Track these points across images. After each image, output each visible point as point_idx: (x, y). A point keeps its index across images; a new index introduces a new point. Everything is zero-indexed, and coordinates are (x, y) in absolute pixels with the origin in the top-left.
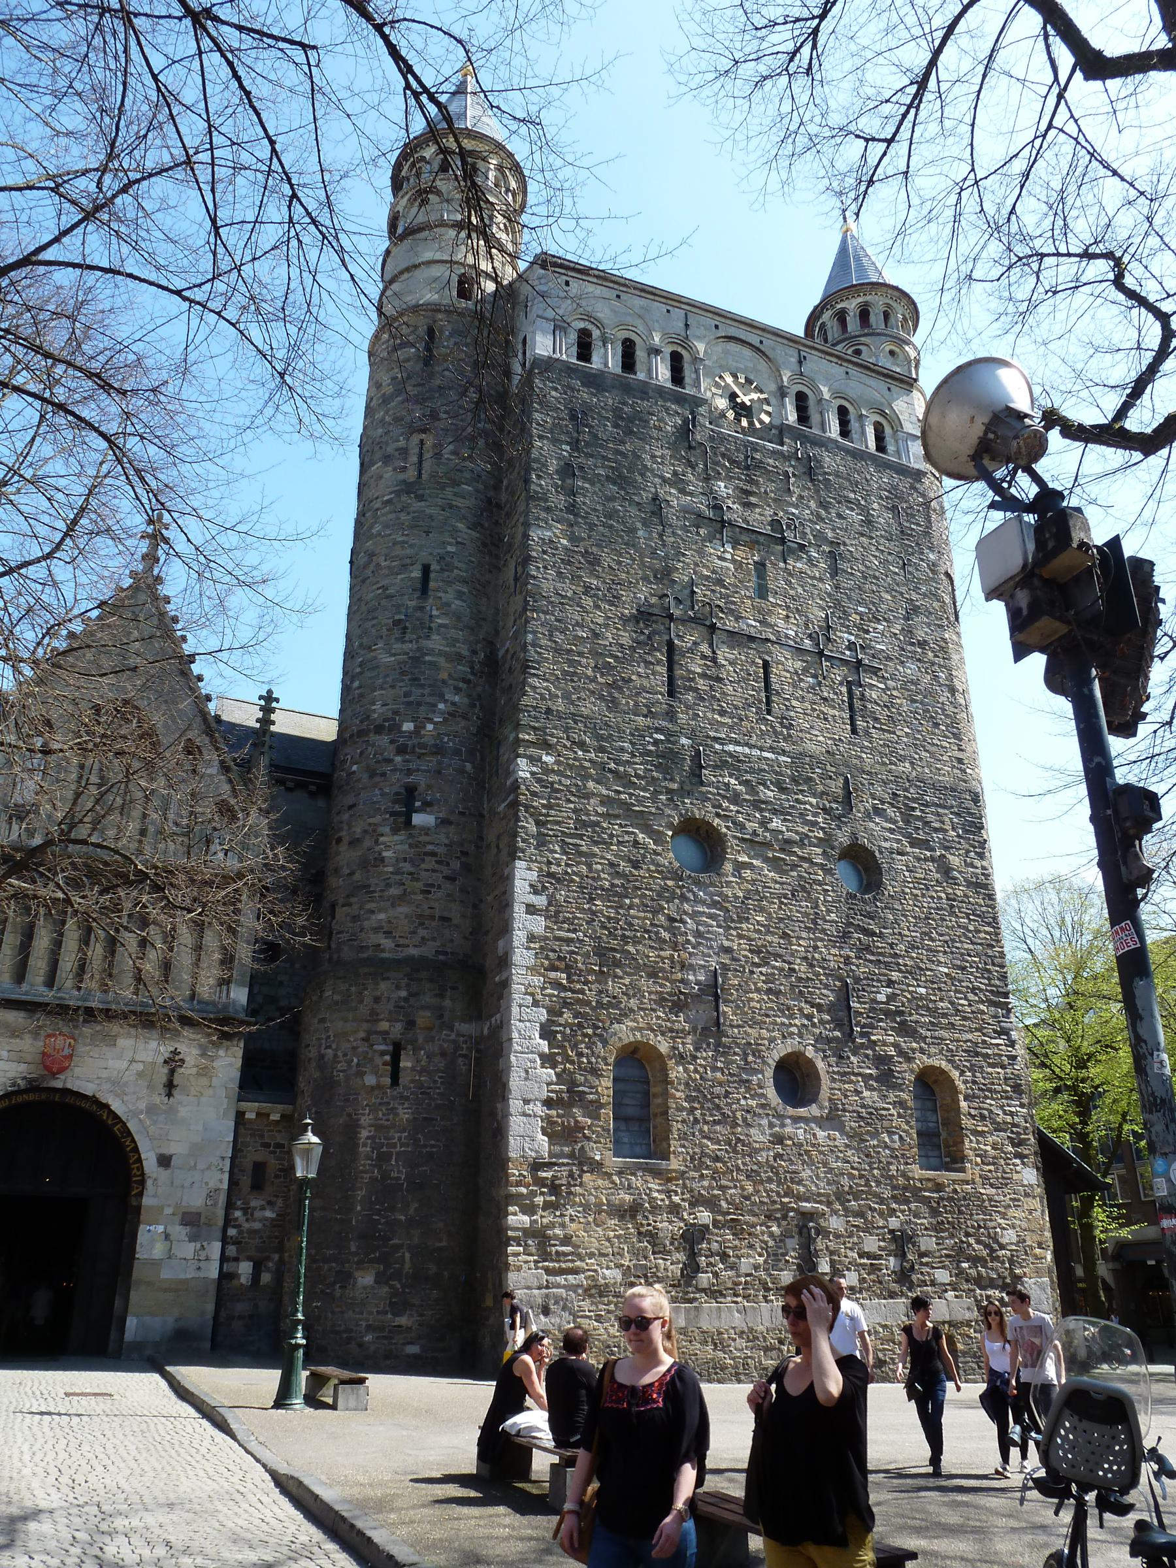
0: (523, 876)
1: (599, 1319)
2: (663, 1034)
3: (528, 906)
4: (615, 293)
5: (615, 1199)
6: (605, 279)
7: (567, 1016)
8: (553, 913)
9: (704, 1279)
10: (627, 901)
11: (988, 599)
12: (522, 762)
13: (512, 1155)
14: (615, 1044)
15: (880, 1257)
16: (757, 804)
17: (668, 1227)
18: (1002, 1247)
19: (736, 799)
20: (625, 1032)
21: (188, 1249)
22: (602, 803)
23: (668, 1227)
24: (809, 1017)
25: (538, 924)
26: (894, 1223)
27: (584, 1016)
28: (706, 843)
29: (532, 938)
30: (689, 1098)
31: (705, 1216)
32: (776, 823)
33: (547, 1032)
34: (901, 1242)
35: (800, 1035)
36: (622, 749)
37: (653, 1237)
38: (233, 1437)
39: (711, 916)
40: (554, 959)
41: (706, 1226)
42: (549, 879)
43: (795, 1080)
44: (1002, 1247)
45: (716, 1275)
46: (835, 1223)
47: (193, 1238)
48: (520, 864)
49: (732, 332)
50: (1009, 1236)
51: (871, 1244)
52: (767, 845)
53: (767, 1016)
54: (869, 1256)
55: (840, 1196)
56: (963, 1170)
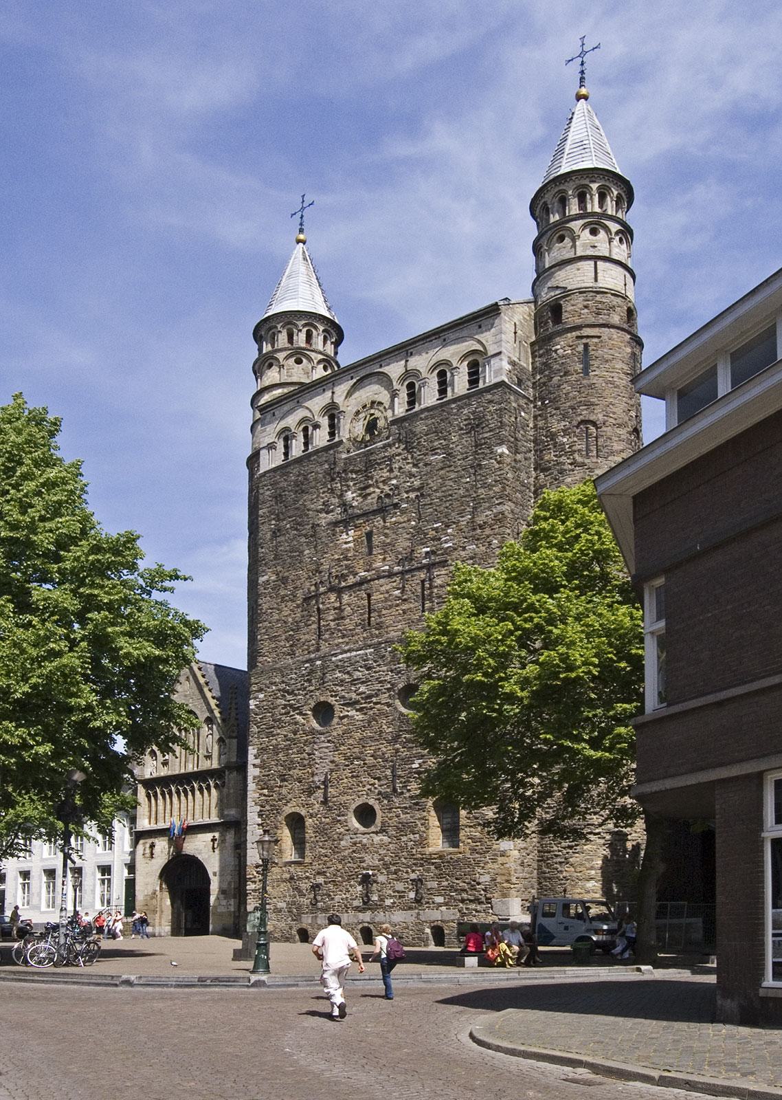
0: (252, 751)
1: (278, 921)
2: (304, 806)
3: (254, 765)
4: (296, 401)
5: (284, 877)
6: (281, 401)
7: (268, 807)
8: (261, 766)
9: (320, 905)
10: (290, 751)
11: (130, 540)
12: (251, 702)
13: (248, 864)
14: (285, 814)
15: (405, 892)
16: (354, 682)
17: (305, 886)
18: (479, 884)
19: (342, 682)
20: (288, 810)
21: (224, 902)
22: (283, 708)
23: (305, 886)
24: (373, 785)
25: (257, 772)
26: (413, 876)
27: (274, 805)
28: (324, 712)
29: (255, 778)
30: (314, 832)
31: (320, 880)
32: (362, 689)
33: (260, 816)
34: (418, 882)
35: (367, 794)
36: (291, 679)
37: (298, 889)
38: (153, 954)
39: (327, 748)
40: (263, 784)
41: (321, 884)
42: (262, 751)
43: (366, 814)
44: (479, 884)
45: (324, 903)
46: (381, 878)
47: (225, 899)
48: (250, 748)
49: (363, 373)
50: (485, 879)
51: (400, 886)
52: (357, 702)
53: (351, 789)
54: (398, 892)
55: (386, 866)
56: (458, 846)
